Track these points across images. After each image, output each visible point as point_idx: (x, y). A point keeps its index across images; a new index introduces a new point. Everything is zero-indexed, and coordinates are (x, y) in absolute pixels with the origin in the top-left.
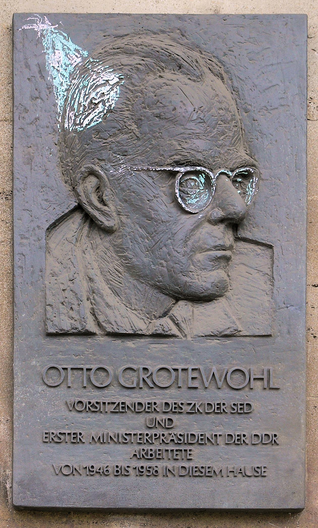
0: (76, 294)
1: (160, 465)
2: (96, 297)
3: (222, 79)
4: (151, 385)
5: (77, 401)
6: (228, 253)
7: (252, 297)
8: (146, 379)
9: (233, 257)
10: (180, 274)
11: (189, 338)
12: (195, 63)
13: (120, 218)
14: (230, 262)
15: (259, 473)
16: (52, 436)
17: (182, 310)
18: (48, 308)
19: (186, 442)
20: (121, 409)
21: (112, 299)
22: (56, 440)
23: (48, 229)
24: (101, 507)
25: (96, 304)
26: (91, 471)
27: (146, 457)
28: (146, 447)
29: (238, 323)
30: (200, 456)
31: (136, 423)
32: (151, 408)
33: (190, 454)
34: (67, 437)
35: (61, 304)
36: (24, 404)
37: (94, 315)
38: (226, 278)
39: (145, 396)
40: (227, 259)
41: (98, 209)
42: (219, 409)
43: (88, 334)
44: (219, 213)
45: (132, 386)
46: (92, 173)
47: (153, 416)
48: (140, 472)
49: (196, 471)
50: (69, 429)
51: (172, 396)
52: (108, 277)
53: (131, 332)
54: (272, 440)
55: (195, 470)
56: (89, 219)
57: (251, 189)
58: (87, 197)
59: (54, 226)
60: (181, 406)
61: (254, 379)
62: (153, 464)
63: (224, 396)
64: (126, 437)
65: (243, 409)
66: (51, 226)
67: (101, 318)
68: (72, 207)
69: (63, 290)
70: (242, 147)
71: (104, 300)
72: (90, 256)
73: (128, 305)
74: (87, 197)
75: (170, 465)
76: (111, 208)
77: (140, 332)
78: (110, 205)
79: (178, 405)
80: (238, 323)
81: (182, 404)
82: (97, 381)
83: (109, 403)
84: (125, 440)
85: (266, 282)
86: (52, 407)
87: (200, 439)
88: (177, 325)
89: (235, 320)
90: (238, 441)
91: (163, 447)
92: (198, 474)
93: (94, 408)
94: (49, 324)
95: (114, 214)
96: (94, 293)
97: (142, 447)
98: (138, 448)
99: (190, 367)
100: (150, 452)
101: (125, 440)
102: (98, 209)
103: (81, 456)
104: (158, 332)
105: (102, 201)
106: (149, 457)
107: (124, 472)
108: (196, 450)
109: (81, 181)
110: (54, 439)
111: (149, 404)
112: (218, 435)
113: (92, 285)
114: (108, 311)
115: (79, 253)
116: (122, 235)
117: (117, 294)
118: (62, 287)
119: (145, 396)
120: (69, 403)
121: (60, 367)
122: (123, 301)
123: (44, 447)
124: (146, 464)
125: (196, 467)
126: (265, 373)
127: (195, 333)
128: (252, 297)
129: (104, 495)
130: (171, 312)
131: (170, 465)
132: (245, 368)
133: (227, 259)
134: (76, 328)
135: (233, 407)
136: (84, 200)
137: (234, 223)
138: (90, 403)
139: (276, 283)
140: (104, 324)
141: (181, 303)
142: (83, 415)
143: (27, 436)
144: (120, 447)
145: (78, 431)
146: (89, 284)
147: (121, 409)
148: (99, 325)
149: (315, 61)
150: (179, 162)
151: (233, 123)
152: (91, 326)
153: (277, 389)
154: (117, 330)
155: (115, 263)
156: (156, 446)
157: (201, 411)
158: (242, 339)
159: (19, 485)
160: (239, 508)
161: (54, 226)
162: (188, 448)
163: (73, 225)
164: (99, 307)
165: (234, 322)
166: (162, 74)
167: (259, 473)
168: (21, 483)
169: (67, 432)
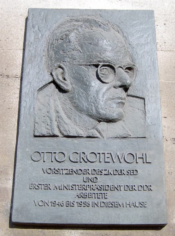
0: (50, 118)
1: (90, 201)
2: (59, 120)
3: (119, 32)
4: (86, 161)
5: (48, 168)
6: (123, 101)
7: (136, 120)
8: (84, 158)
9: (126, 103)
10: (101, 109)
11: (105, 138)
12: (106, 24)
13: (72, 86)
14: (124, 106)
15: (142, 205)
16: (34, 185)
17: (103, 126)
18: (36, 124)
19: (104, 189)
20: (71, 172)
21: (67, 121)
22: (36, 187)
23: (38, 90)
24: (59, 223)
25: (60, 122)
26: (54, 204)
27: (83, 197)
28: (84, 192)
29: (129, 131)
30: (112, 196)
31: (78, 180)
32: (86, 172)
33: (106, 196)
34: (43, 186)
35: (42, 122)
36: (21, 170)
37: (59, 128)
38: (123, 112)
39: (84, 166)
40: (123, 104)
41: (62, 82)
42: (121, 173)
43: (54, 136)
44: (119, 83)
45: (76, 161)
46: (60, 67)
47: (88, 176)
48: (80, 204)
49: (110, 204)
50: (43, 182)
51: (98, 166)
52: (66, 111)
53: (76, 135)
54: (149, 188)
55: (109, 203)
56: (58, 87)
57: (97, 148)
58: (57, 76)
59: (41, 89)
60: (101, 171)
61: (139, 158)
62: (87, 200)
63: (125, 167)
64: (73, 186)
65: (133, 173)
66: (40, 89)
67: (62, 129)
68: (50, 81)
69: (44, 116)
70: (128, 58)
71: (63, 121)
72: (58, 103)
73: (75, 124)
74: (57, 76)
75: (96, 201)
76: (68, 82)
77: (81, 136)
78: (68, 80)
79: (100, 171)
80: (129, 131)
81: (102, 170)
82: (59, 159)
83: (64, 169)
84: (73, 187)
85: (142, 114)
86: (31, 171)
87: (111, 187)
88: (99, 133)
89: (128, 130)
90: (131, 188)
91: (92, 192)
92: (111, 205)
93: (57, 172)
94: (36, 131)
95: (70, 84)
96: (59, 118)
97: (81, 191)
98: (79, 192)
99: (80, 184)
100: (85, 194)
101: (73, 187)
102: (62, 82)
103: (50, 196)
104: (90, 135)
105: (64, 79)
106: (85, 197)
107: (72, 205)
108: (109, 193)
109: (54, 70)
110: (35, 187)
111: (85, 170)
112: (76, 185)
113: (58, 114)
114: (65, 126)
115: (52, 101)
116: (73, 93)
117: (70, 118)
118: (43, 115)
119: (84, 166)
120: (44, 169)
121: (40, 152)
122: (72, 122)
123: (30, 192)
124: (83, 200)
125: (110, 202)
126: (144, 155)
127: (108, 136)
128: (136, 120)
129: (61, 217)
130: (96, 127)
131: (96, 201)
132: (134, 153)
133: (123, 104)
134: (49, 133)
135: (128, 171)
136: (55, 77)
137: (125, 88)
138: (55, 169)
139: (147, 114)
140: (63, 132)
141: (101, 123)
142: (51, 175)
143: (22, 186)
144: (70, 192)
145: (48, 183)
146: (57, 114)
147: (71, 172)
148: (61, 132)
149: (54, 231)
150: (99, 61)
151: (124, 48)
152: (57, 132)
153: (150, 163)
154: (69, 135)
155: (69, 105)
156: (89, 191)
157: (112, 174)
158: (131, 139)
159: (15, 211)
160: (133, 224)
161: (41, 89)
162: (105, 192)
163: (50, 89)
164: (61, 124)
165: (127, 131)
166: (92, 28)
167: (142, 205)
168: (17, 210)
169: (42, 184)
